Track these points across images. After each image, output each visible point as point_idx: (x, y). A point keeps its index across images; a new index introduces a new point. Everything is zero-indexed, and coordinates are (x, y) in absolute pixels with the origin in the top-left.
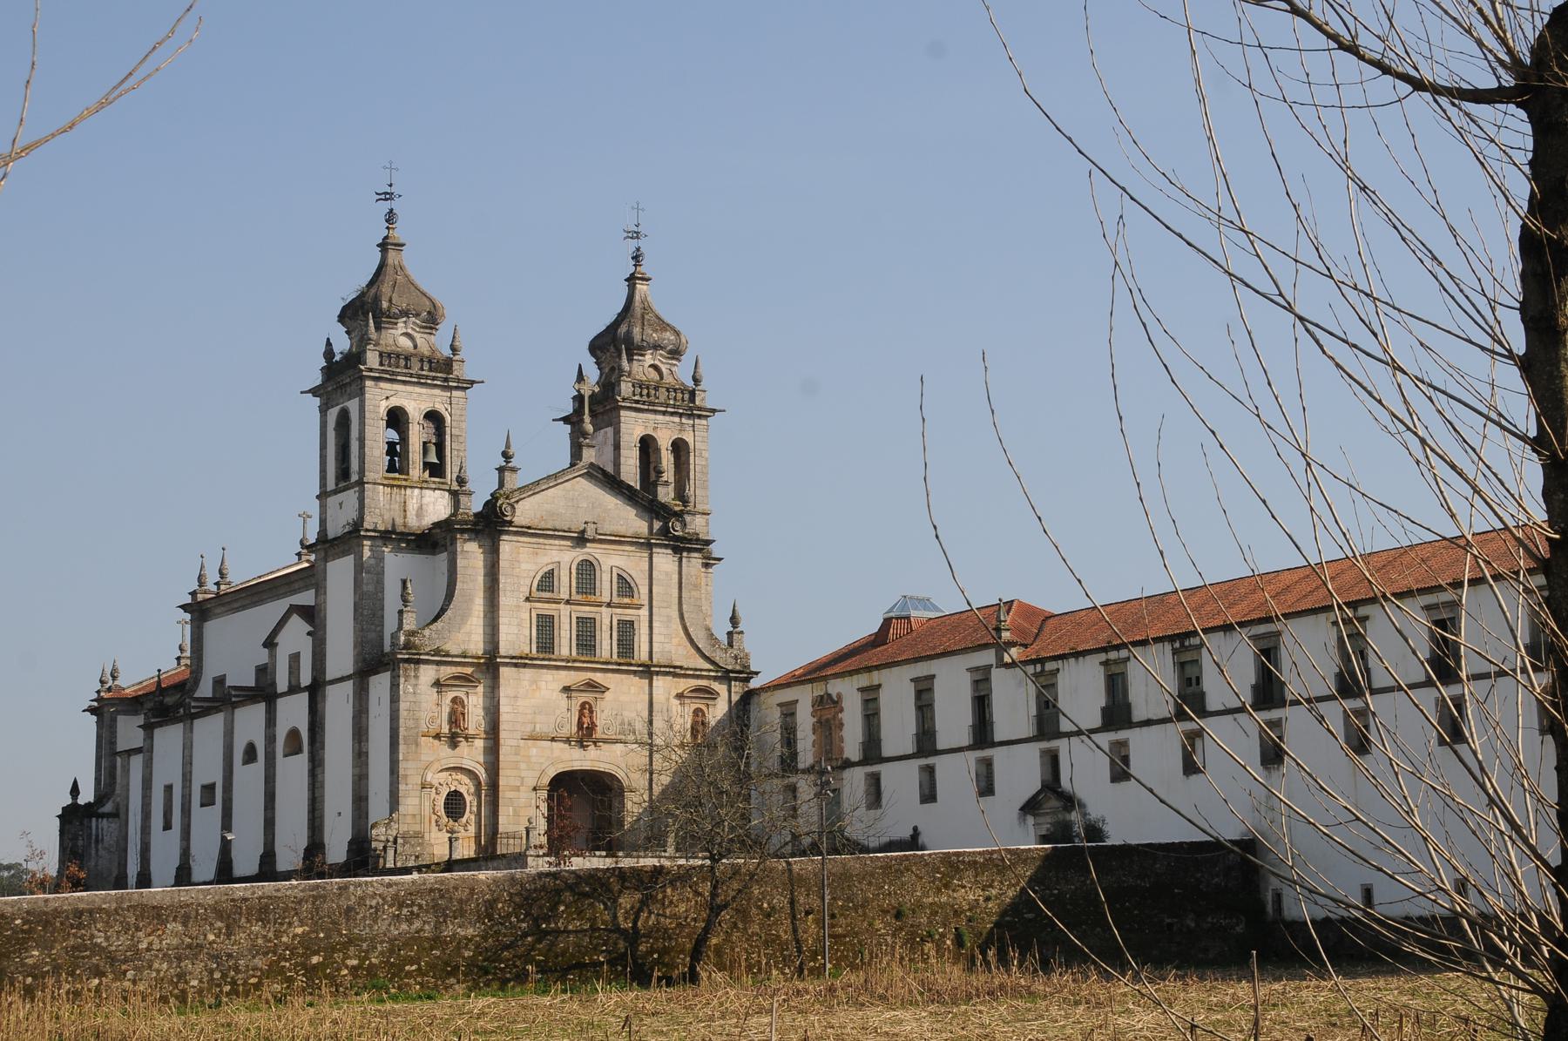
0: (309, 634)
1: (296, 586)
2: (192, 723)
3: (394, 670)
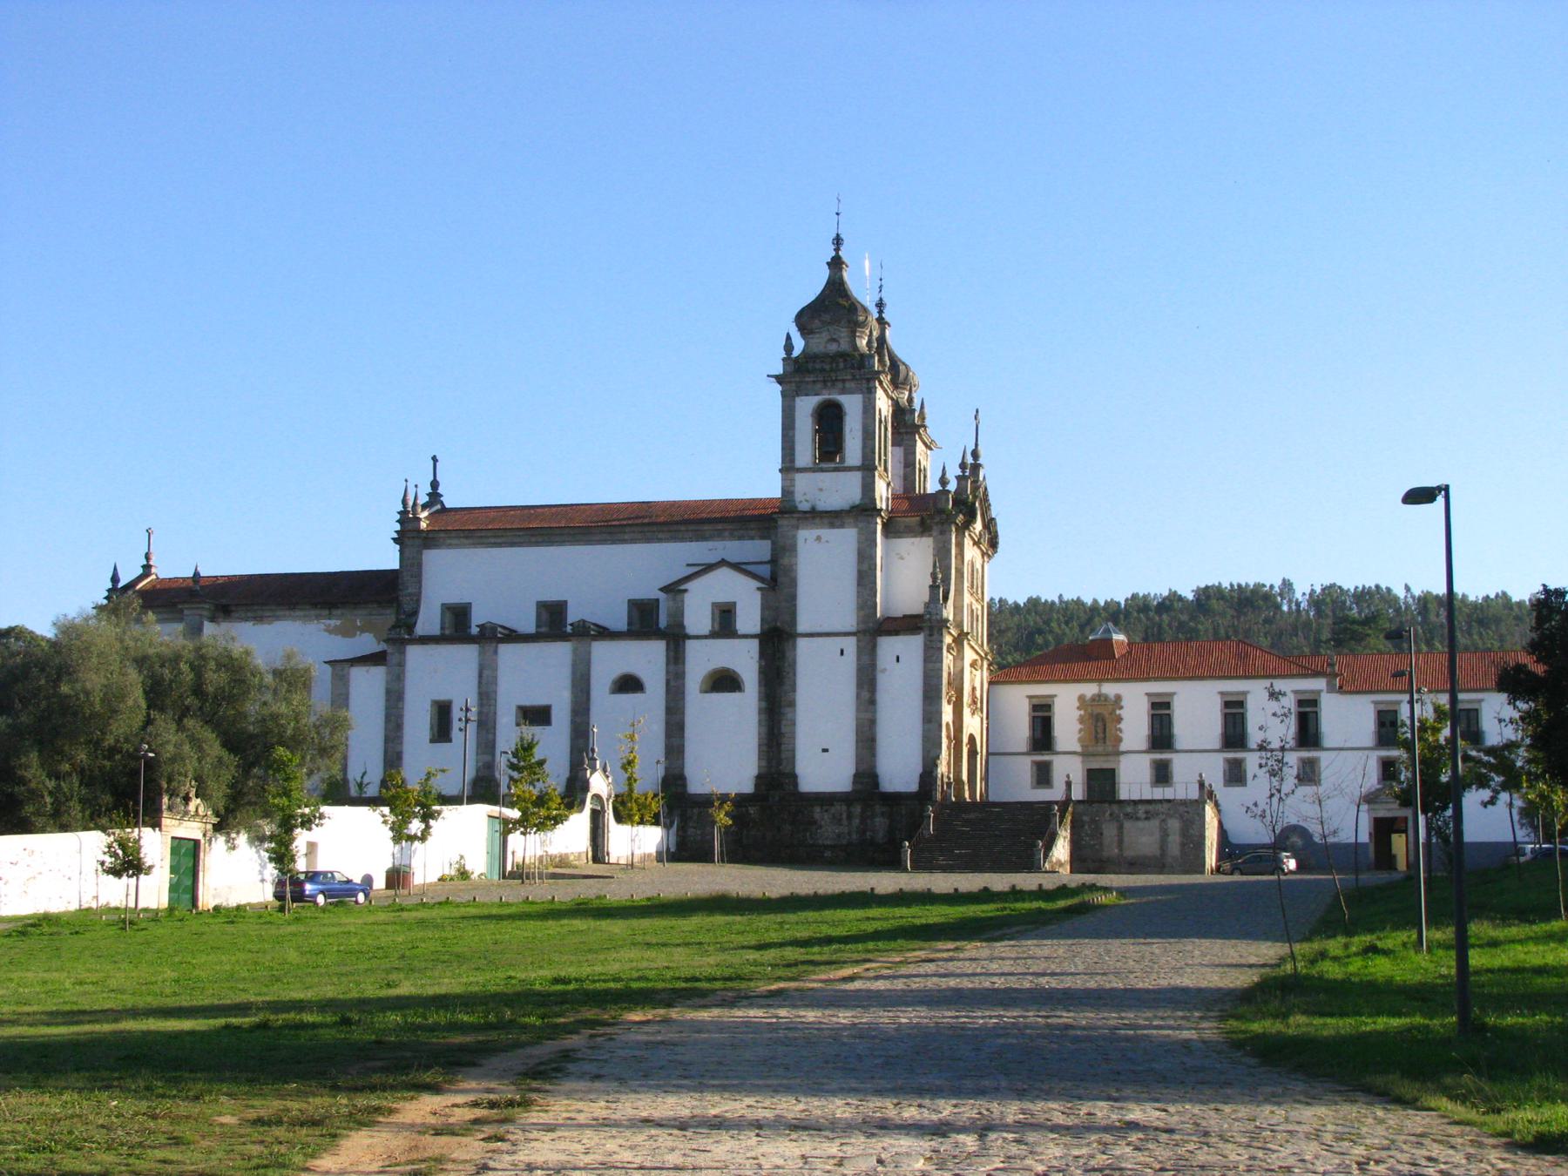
0: (758, 589)
1: (626, 537)
2: (497, 647)
3: (931, 635)
